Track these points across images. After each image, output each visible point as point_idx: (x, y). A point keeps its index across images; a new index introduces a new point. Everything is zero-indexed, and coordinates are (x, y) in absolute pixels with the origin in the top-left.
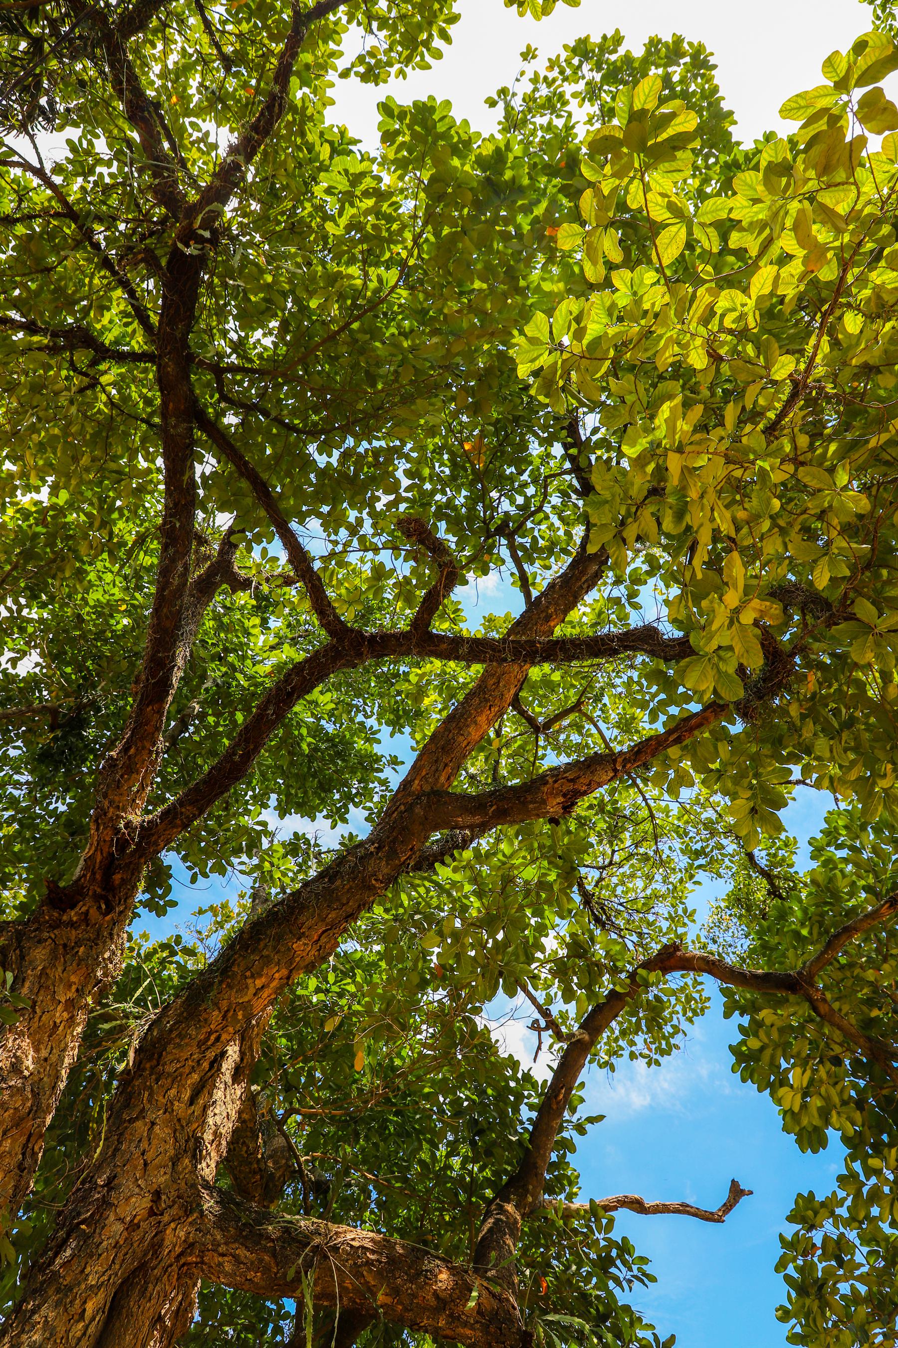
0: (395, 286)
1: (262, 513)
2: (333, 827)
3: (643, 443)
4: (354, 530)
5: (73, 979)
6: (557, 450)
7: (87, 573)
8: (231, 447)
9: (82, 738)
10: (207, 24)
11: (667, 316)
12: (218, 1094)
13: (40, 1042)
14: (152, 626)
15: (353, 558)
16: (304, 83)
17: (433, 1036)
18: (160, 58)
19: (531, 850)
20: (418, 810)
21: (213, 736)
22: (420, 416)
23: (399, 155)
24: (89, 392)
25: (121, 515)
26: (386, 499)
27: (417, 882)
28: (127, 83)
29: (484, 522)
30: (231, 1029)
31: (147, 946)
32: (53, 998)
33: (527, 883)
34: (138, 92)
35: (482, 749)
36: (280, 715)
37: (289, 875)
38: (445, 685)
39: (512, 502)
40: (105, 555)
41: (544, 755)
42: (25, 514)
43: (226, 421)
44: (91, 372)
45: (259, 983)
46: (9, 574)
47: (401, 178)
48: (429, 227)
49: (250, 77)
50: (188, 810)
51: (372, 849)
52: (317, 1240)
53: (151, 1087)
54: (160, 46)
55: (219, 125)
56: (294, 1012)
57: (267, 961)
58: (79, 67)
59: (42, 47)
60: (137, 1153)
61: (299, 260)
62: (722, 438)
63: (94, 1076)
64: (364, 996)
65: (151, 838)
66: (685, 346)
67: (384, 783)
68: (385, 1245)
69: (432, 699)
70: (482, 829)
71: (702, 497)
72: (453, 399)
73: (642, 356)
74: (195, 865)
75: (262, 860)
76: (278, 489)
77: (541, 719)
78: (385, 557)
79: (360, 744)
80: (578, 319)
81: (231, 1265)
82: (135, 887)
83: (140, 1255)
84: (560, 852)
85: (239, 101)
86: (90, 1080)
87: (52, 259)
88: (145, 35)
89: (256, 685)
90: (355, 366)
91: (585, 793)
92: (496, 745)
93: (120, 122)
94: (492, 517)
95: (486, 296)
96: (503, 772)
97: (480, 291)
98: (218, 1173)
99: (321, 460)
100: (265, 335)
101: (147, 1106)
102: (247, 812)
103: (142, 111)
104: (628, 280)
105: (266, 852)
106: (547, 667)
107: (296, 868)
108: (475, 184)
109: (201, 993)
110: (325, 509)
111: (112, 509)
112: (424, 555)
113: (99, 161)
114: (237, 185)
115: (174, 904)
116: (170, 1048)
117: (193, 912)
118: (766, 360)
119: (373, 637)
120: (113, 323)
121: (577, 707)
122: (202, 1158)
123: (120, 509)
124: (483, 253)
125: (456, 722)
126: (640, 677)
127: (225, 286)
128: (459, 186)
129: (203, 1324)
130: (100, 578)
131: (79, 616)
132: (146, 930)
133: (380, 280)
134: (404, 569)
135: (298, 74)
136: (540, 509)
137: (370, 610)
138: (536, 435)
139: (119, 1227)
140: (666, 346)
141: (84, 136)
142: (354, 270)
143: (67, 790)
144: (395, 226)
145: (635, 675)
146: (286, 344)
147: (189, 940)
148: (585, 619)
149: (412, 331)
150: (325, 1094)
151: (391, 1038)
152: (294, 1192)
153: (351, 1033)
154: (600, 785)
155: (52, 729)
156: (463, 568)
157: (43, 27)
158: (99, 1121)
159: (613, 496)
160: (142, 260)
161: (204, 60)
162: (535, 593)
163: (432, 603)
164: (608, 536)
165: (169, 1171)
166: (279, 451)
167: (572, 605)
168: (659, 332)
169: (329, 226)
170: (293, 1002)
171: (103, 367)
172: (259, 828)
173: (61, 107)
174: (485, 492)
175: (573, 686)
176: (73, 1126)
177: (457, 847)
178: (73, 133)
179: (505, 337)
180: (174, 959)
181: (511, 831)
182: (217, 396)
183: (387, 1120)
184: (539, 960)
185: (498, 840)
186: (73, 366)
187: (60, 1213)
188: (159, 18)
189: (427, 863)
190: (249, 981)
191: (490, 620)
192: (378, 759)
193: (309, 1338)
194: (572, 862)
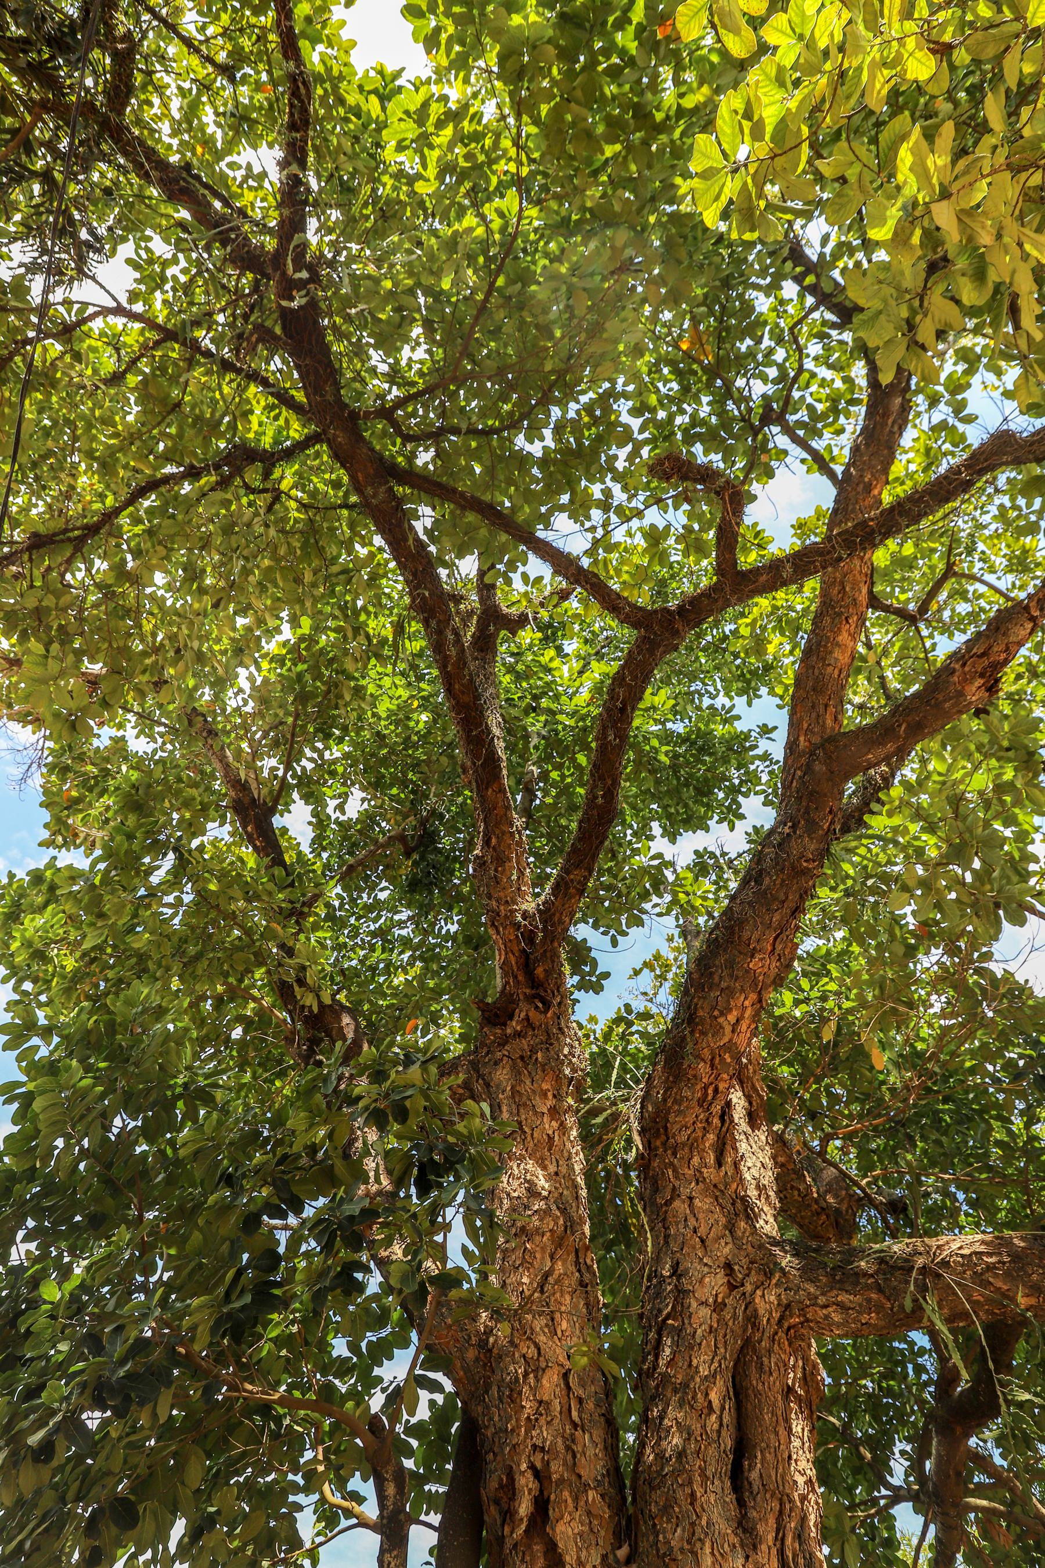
0: (521, 210)
1: (504, 537)
2: (732, 829)
3: (894, 213)
4: (605, 506)
5: (545, 1086)
6: (790, 289)
7: (364, 688)
8: (439, 485)
9: (439, 851)
10: (187, 42)
11: (857, 37)
12: (743, 1147)
13: (543, 1159)
14: (453, 708)
15: (619, 535)
16: (315, 41)
17: (948, 1003)
18: (161, 114)
19: (969, 756)
20: (818, 767)
21: (565, 791)
22: (616, 342)
23: (453, 56)
24: (277, 506)
25: (368, 614)
26: (623, 453)
27: (854, 844)
28: (146, 161)
29: (743, 420)
30: (725, 1076)
31: (600, 1028)
32: (536, 1113)
33: (981, 793)
34: (162, 165)
35: (859, 671)
36: (623, 736)
37: (710, 898)
38: (787, 625)
39: (765, 379)
40: (373, 661)
41: (934, 645)
42: (280, 660)
43: (419, 462)
44: (269, 486)
45: (732, 1018)
46: (295, 725)
47: (466, 81)
48: (525, 118)
49: (258, 73)
50: (576, 875)
51: (787, 830)
52: (920, 1261)
53: (672, 1164)
54: (156, 100)
55: (255, 147)
56: (783, 1037)
57: (730, 992)
58: (96, 177)
59: (53, 178)
60: (688, 1232)
61: (407, 246)
62: (996, 147)
63: (609, 1173)
64: (850, 990)
65: (554, 919)
66: (898, 60)
67: (766, 757)
68: (1000, 1244)
69: (776, 644)
70: (901, 755)
71: (999, 237)
72: (644, 301)
73: (845, 109)
74: (609, 927)
75: (675, 894)
76: (507, 504)
77: (911, 606)
78: (653, 516)
79: (719, 730)
80: (748, 115)
81: (838, 1313)
82: (561, 974)
83: (739, 1332)
84: (1005, 743)
85: (261, 108)
86: (607, 1178)
87: (175, 392)
88: (137, 98)
89: (583, 719)
90: (522, 326)
91: (1006, 662)
92: (872, 659)
93: (163, 209)
94: (750, 410)
95: (625, 158)
96: (894, 685)
97: (616, 156)
98: (780, 1228)
99: (536, 449)
100: (413, 349)
101: (677, 1183)
102: (636, 852)
103: (180, 183)
104: (786, 24)
105: (673, 884)
106: (892, 544)
107: (713, 888)
108: (550, 32)
109: (674, 1052)
110: (565, 498)
111: (356, 613)
112: (695, 490)
113: (165, 264)
114: (306, 203)
115: (606, 975)
116: (672, 1117)
117: (628, 975)
118: (1013, 8)
119: (681, 608)
120: (264, 424)
121: (949, 571)
122: (757, 1217)
123: (364, 608)
124: (599, 110)
125: (815, 654)
126: (1013, 499)
127: (348, 319)
128: (534, 47)
129: (837, 1384)
130: (380, 687)
131: (378, 733)
132: (592, 1010)
133: (501, 214)
134: (678, 518)
135: (304, 35)
136: (800, 370)
137: (663, 583)
138: (757, 287)
139: (705, 1312)
140: (872, 77)
141: (138, 247)
142: (470, 220)
143: (450, 909)
144: (488, 142)
145: (1006, 500)
146: (440, 345)
147: (639, 1005)
148: (913, 467)
149: (563, 251)
150: (856, 1108)
151: (901, 1023)
152: (869, 1221)
153: (854, 1033)
154: (1021, 644)
155: (408, 855)
156: (743, 483)
157: (44, 157)
158: (637, 1215)
159: (885, 301)
160: (258, 341)
161: (205, 86)
162: (839, 469)
163: (728, 538)
164: (899, 352)
165: (729, 1239)
166: (488, 463)
167: (890, 459)
168: (855, 64)
169: (421, 187)
170: (775, 1025)
171: (277, 474)
172: (656, 862)
173: (102, 231)
174: (728, 385)
175: (933, 551)
176: (614, 1232)
177: (880, 789)
178: (126, 250)
179: (669, 192)
180: (634, 1029)
181: (934, 745)
182: (399, 441)
183: (938, 1111)
184: (1035, 873)
185: (924, 762)
186: (250, 489)
187: (641, 1316)
188: (140, 70)
189: (853, 821)
190: (721, 1020)
191: (801, 526)
192: (747, 736)
193: (960, 1365)
194: (1026, 747)
